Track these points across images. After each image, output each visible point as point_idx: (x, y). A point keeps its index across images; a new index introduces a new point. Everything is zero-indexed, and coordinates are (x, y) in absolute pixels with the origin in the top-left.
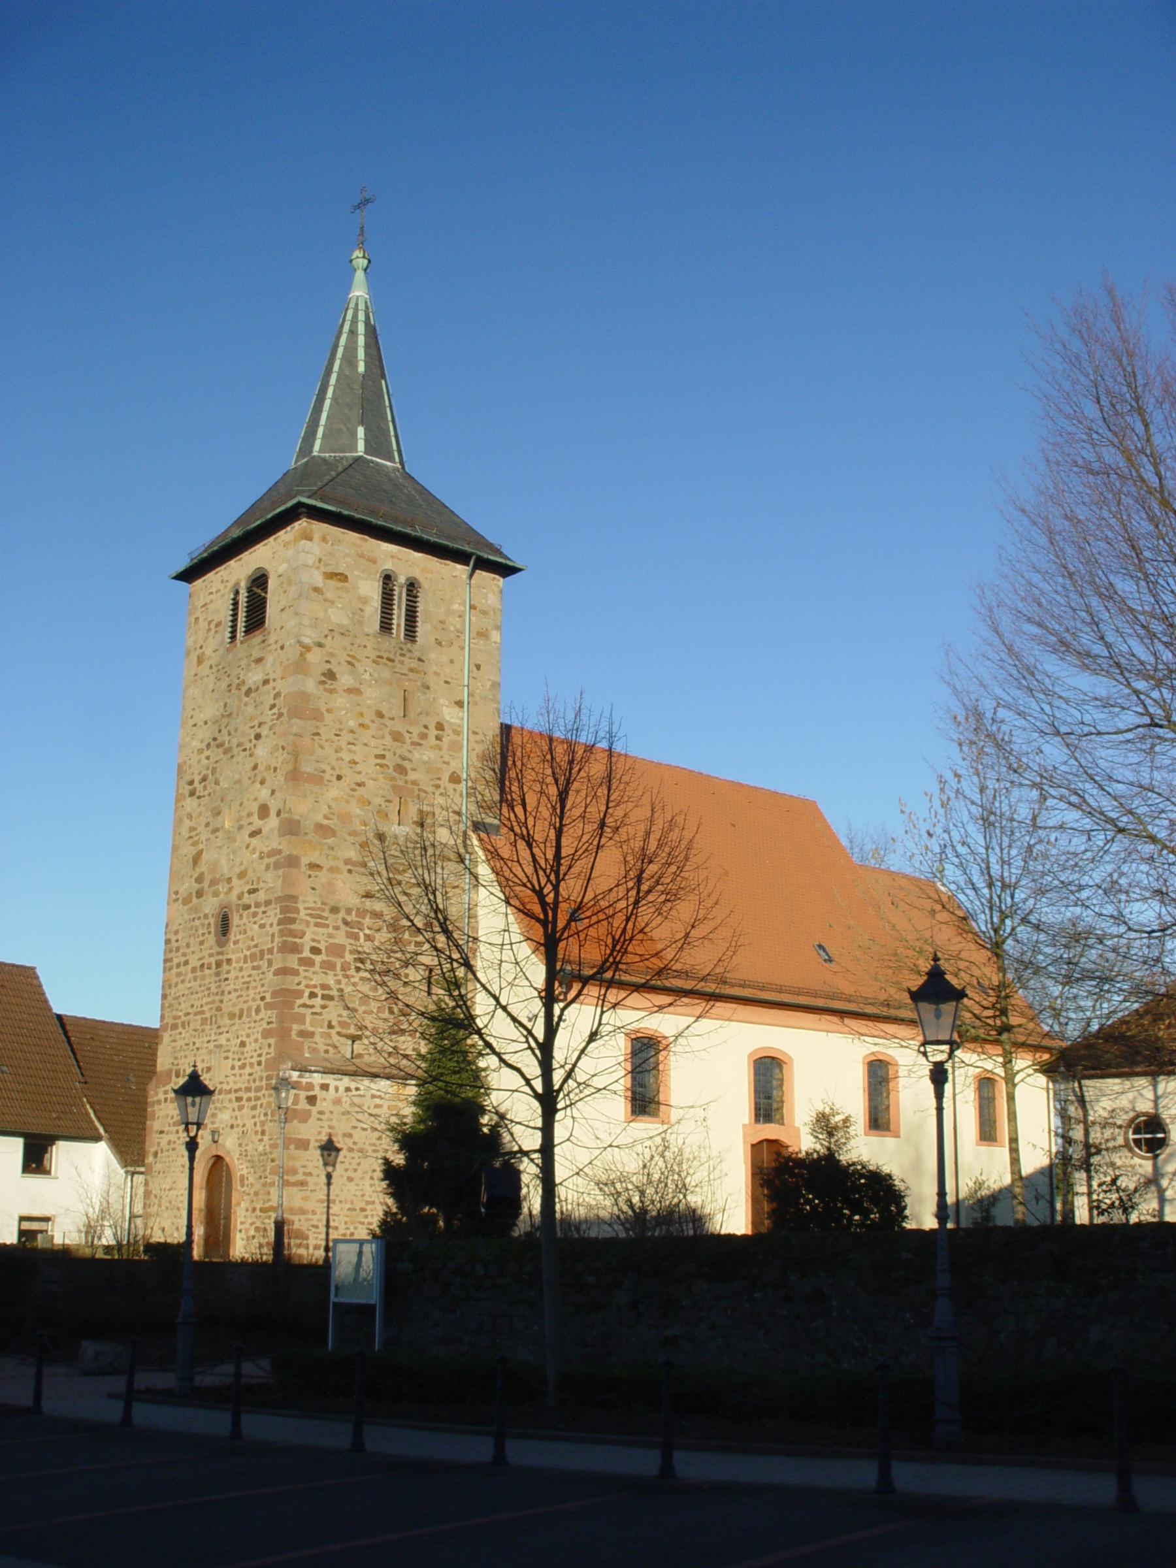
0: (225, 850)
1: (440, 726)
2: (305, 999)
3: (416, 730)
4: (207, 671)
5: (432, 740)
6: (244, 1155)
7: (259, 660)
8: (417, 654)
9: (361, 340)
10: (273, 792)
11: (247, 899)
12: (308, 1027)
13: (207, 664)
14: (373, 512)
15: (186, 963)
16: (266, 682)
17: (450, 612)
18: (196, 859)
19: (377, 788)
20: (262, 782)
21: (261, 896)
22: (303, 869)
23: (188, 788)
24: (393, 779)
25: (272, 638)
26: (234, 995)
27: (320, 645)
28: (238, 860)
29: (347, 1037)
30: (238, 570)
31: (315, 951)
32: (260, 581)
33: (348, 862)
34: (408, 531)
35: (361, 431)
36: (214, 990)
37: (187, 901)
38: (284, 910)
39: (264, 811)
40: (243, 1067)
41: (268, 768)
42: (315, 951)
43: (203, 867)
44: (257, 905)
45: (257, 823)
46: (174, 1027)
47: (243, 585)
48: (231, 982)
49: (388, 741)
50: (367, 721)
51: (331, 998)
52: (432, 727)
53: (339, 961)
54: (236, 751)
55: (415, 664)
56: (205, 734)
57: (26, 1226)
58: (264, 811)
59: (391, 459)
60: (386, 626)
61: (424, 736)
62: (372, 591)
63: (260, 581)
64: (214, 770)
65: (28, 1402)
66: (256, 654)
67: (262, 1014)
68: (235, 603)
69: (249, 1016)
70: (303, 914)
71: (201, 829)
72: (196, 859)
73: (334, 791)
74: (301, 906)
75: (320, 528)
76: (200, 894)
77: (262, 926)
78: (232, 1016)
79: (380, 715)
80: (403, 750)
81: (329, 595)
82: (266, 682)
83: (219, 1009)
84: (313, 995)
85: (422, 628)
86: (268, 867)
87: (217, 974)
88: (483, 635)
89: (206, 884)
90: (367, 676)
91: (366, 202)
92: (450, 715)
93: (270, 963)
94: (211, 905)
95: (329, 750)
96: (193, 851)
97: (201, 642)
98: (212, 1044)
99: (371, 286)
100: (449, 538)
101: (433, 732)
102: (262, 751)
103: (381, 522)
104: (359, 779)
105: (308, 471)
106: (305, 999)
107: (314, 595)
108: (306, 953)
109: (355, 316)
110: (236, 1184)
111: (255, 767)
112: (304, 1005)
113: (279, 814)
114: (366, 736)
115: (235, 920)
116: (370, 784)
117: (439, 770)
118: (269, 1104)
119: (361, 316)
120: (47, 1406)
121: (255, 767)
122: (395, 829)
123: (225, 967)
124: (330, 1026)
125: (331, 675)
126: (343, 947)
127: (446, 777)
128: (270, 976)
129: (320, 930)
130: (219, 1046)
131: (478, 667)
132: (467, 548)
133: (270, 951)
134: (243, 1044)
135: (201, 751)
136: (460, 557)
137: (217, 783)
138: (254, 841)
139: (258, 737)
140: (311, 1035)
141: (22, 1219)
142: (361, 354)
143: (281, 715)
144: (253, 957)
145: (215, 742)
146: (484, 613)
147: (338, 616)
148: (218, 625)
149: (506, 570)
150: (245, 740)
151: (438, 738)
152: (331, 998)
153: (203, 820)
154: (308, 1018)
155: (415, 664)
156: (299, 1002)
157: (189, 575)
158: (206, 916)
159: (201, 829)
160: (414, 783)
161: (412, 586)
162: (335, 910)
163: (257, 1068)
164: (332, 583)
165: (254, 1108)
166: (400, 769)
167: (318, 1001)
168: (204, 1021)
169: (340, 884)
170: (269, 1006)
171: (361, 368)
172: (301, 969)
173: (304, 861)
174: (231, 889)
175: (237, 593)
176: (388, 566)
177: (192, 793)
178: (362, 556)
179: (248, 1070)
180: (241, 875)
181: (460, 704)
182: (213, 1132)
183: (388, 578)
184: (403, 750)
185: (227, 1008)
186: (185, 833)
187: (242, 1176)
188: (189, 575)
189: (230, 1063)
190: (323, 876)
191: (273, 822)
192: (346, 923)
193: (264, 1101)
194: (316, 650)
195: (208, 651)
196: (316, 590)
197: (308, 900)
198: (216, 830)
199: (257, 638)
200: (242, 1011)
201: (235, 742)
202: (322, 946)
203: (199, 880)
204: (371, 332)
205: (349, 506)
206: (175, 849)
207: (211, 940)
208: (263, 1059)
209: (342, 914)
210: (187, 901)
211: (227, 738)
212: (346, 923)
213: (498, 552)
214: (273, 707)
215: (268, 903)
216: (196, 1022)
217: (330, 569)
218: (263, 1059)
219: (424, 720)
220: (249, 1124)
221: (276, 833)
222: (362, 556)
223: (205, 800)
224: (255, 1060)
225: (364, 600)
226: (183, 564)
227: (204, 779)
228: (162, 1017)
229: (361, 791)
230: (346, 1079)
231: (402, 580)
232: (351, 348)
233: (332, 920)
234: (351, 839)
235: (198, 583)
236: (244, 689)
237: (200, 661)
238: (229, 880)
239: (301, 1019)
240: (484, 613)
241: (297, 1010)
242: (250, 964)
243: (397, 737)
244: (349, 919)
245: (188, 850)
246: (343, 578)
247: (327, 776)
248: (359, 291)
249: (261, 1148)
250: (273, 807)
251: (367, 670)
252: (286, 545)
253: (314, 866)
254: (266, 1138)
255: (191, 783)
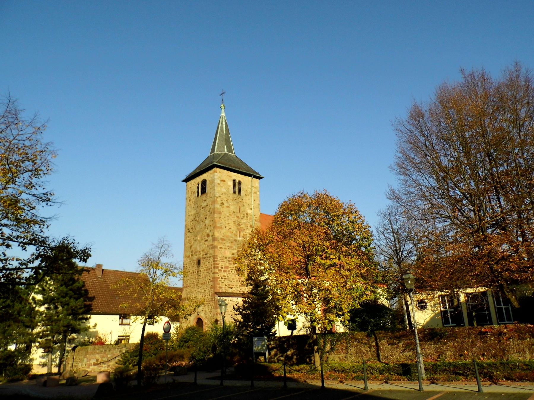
0: (198, 245)
1: (247, 214)
2: (220, 279)
3: (242, 215)
4: (192, 203)
5: (245, 218)
6: (206, 317)
7: (205, 200)
8: (241, 198)
9: (224, 126)
10: (210, 231)
11: (205, 256)
12: (221, 286)
13: (191, 201)
14: (230, 166)
15: (189, 272)
16: (207, 205)
17: (248, 188)
18: (191, 247)
19: (234, 229)
20: (207, 229)
21: (208, 255)
22: (219, 248)
23: (188, 231)
24: (237, 227)
25: (208, 195)
26: (202, 279)
27: (220, 197)
28: (202, 247)
29: (230, 288)
30: (199, 179)
31: (222, 268)
32: (204, 182)
33: (228, 246)
34: (238, 170)
35: (225, 147)
36: (197, 278)
37: (189, 257)
38: (214, 259)
39: (208, 235)
40: (205, 296)
41: (209, 225)
42: (222, 268)
43: (193, 249)
44: (207, 257)
45: (207, 238)
46: (186, 287)
47: (200, 183)
48: (201, 276)
49: (236, 218)
50: (231, 214)
51: (226, 279)
52: (245, 215)
53: (227, 270)
54: (200, 222)
55: (241, 200)
56: (192, 218)
57: (120, 338)
58: (208, 235)
59: (233, 153)
60: (234, 192)
61: (244, 217)
62: (231, 184)
63: (204, 182)
64: (194, 226)
65: (193, 381)
66: (204, 199)
67: (210, 283)
68: (198, 187)
69: (206, 284)
70: (219, 259)
71: (192, 240)
72: (191, 247)
73: (224, 231)
74: (218, 258)
75: (219, 170)
76: (192, 255)
77: (209, 262)
78: (202, 284)
79: (234, 212)
80: (239, 220)
81: (222, 185)
82: (207, 205)
83: (198, 282)
84: (222, 278)
85: (242, 192)
86: (210, 249)
87: (198, 274)
88: (255, 193)
89: (194, 253)
90: (230, 203)
91: (224, 93)
92: (249, 212)
93: (211, 271)
94: (195, 258)
95: (223, 221)
96: (190, 245)
97: (190, 196)
98: (197, 291)
99: (226, 113)
100: (247, 171)
101: (246, 216)
102: (207, 221)
103: (232, 168)
104: (230, 227)
105: (213, 157)
106: (220, 279)
107: (218, 185)
108: (220, 268)
109: (222, 120)
110: (204, 324)
111: (205, 225)
112: (220, 281)
113: (212, 236)
114: (231, 217)
115: (202, 261)
116: (232, 228)
117: (247, 224)
118: (212, 305)
119: (224, 120)
120: (197, 382)
121: (205, 225)
122: (238, 238)
123: (200, 272)
124: (226, 285)
125: (223, 204)
126: (228, 267)
127: (249, 226)
128: (211, 274)
129: (223, 263)
130: (199, 291)
131: (255, 200)
132: (251, 173)
133: (211, 268)
134: (205, 291)
135: (191, 222)
136: (250, 175)
137: (196, 229)
138: (206, 243)
139: (206, 218)
140: (222, 288)
141: (119, 336)
142: (224, 129)
143: (211, 213)
144: (207, 270)
145: (194, 219)
146: (256, 188)
147: (224, 190)
148: (194, 192)
149: (260, 178)
150: (202, 219)
151: (247, 217)
152: (226, 279)
153: (192, 238)
154: (221, 284)
155: (241, 200)
156: (219, 280)
157: (187, 180)
158: (194, 260)
159: (192, 240)
160: (242, 228)
161: (240, 182)
162: (226, 258)
163: (209, 296)
164: (222, 182)
165: (208, 306)
166: (239, 225)
167: (223, 280)
168: (194, 286)
169: (226, 252)
170: (211, 281)
171: (225, 132)
172: (219, 272)
173: (219, 247)
174: (200, 254)
175: (198, 185)
176: (234, 178)
177: (189, 232)
178: (228, 176)
179: (207, 297)
180: (203, 251)
181: (251, 209)
182: (198, 312)
183: (234, 181)
184: (239, 220)
185: (200, 282)
186: (188, 241)
187: (206, 323)
188: (187, 180)
189: (202, 295)
190: (223, 250)
191: (211, 238)
192: (228, 261)
193: (211, 304)
194: (219, 198)
195: (192, 198)
196: (219, 184)
197: (219, 256)
198: (196, 240)
199: (204, 195)
200: (204, 283)
201: (200, 220)
202: (223, 267)
203: (192, 252)
204: (226, 124)
205: (224, 165)
206: (185, 244)
207: (196, 266)
208: (210, 294)
209: (228, 259)
210: (189, 257)
211: (197, 219)
212: (228, 261)
213: (258, 174)
214: (209, 211)
215: (210, 257)
216: (192, 286)
217: (222, 179)
218: (210, 294)
219: (244, 213)
220: (207, 310)
221: (211, 241)
222: (228, 176)
223: (192, 233)
224: (208, 294)
225: (230, 186)
226: (184, 178)
227: (192, 228)
228: (183, 285)
229: (231, 230)
230: (230, 298)
231: (237, 181)
232: (222, 128)
233: (225, 260)
234: (229, 241)
235: (188, 183)
236: (201, 207)
237: (190, 201)
238: (200, 252)
239: (219, 284)
240: (256, 188)
241: (218, 282)
242: (206, 271)
243: (238, 217)
244: (229, 260)
245: (189, 245)
246: (224, 181)
247: (223, 227)
248: (223, 114)
249: (210, 316)
250: (211, 234)
251: (231, 202)
252: (211, 174)
253: (221, 248)
254: (212, 313)
255: (189, 229)
